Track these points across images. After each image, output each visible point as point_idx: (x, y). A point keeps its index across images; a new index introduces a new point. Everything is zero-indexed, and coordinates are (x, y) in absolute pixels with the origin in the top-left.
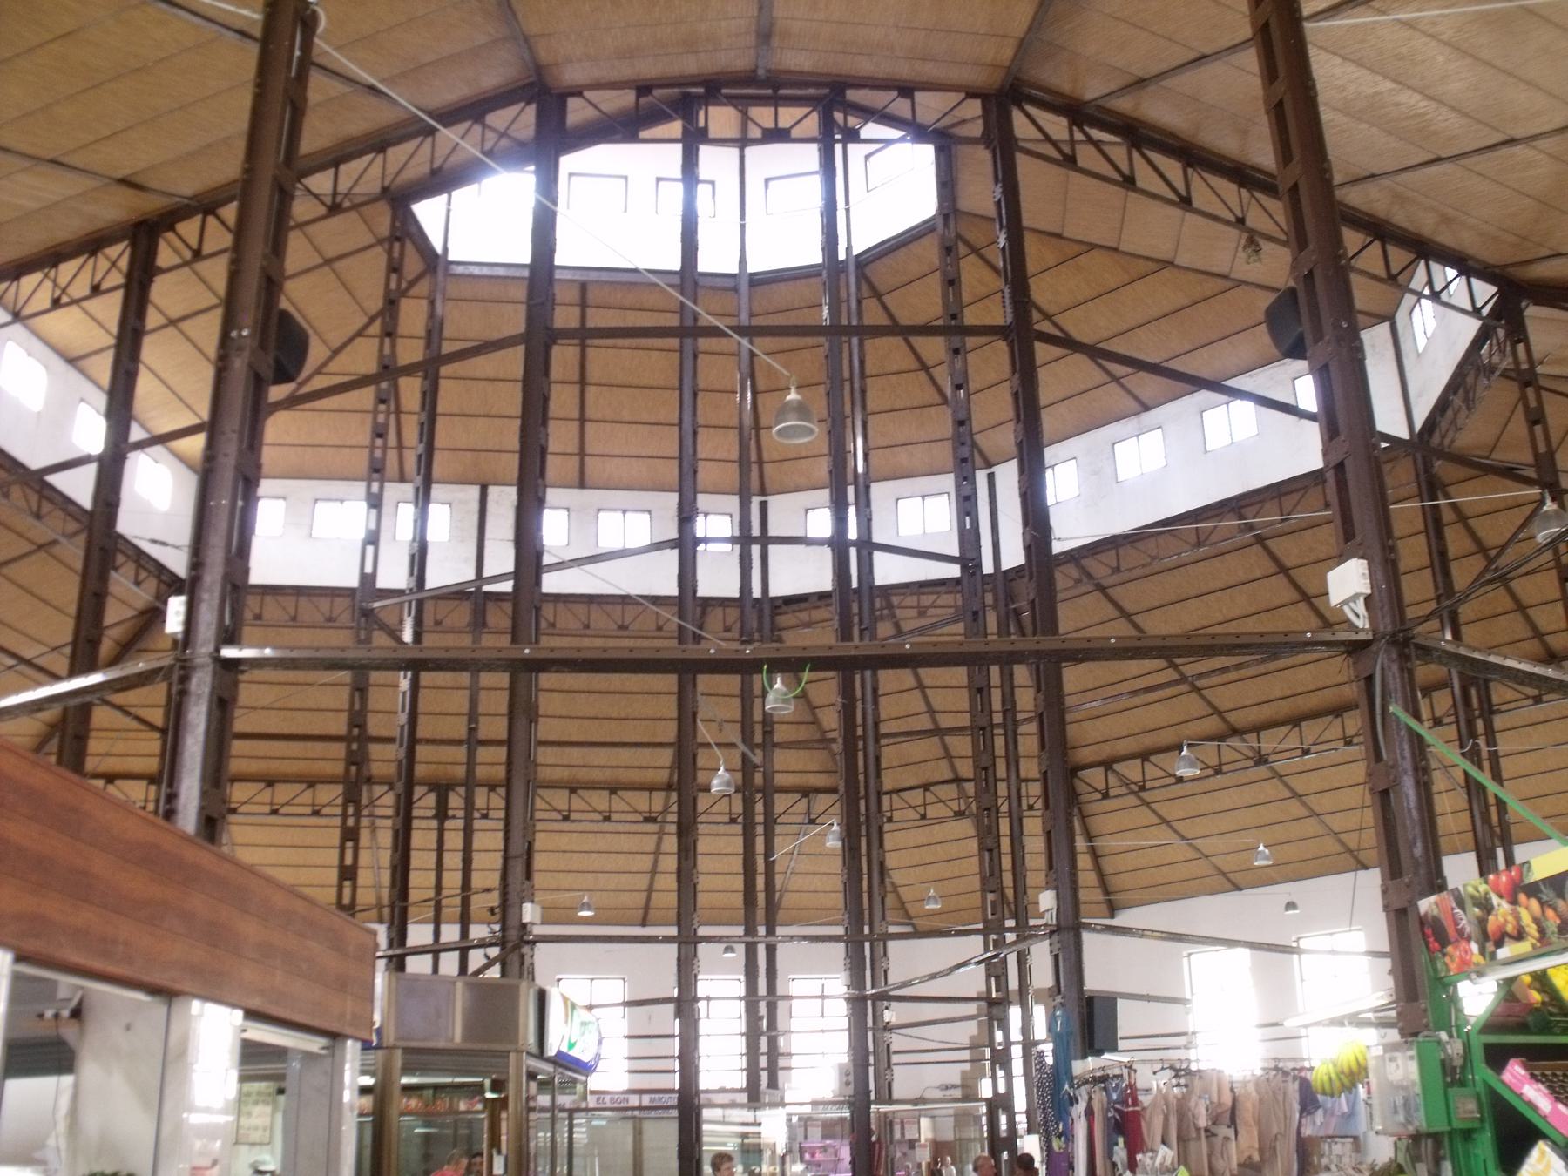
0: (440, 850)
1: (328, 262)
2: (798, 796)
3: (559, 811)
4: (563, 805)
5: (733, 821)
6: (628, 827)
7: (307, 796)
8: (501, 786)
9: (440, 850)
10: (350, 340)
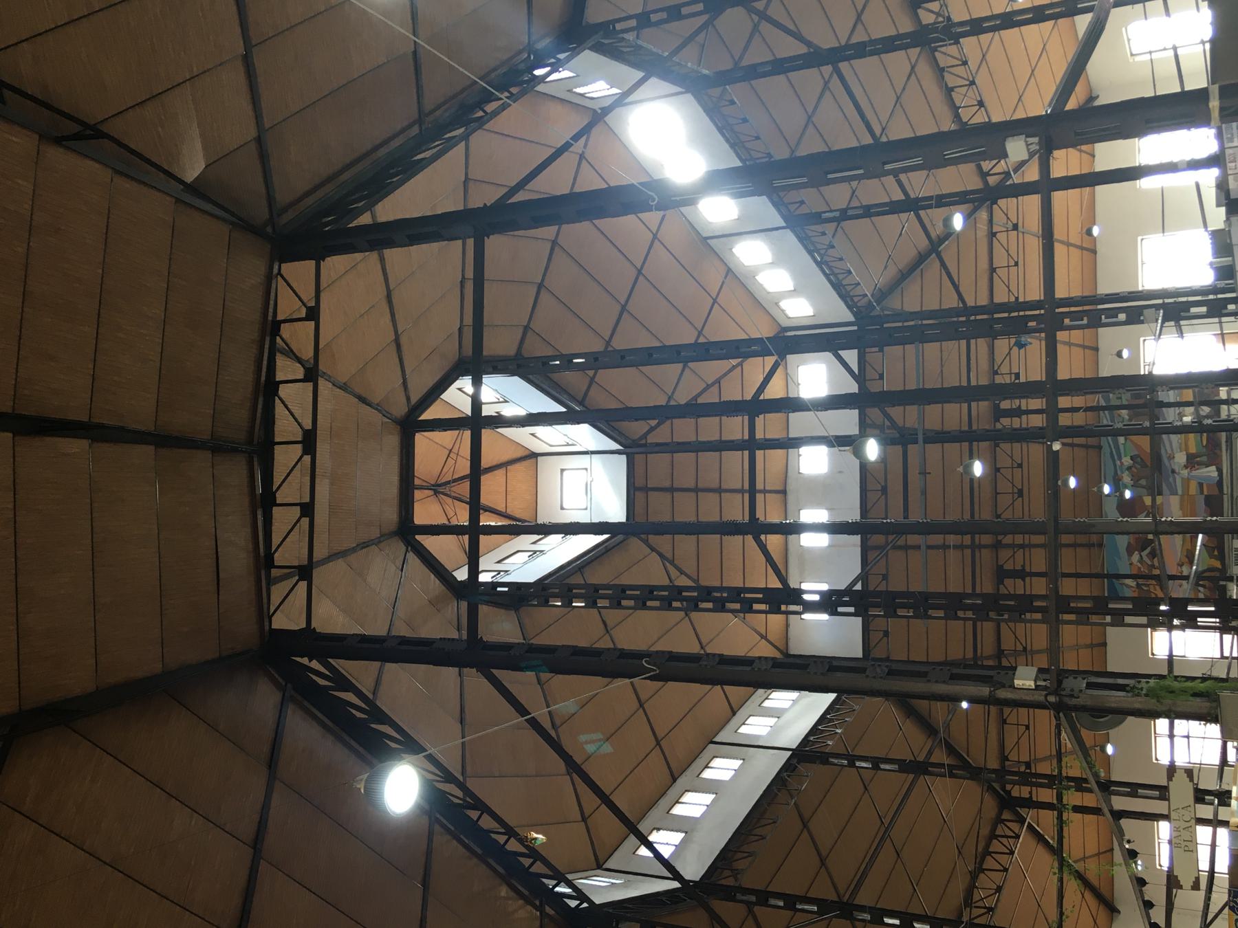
7: (1002, 273)
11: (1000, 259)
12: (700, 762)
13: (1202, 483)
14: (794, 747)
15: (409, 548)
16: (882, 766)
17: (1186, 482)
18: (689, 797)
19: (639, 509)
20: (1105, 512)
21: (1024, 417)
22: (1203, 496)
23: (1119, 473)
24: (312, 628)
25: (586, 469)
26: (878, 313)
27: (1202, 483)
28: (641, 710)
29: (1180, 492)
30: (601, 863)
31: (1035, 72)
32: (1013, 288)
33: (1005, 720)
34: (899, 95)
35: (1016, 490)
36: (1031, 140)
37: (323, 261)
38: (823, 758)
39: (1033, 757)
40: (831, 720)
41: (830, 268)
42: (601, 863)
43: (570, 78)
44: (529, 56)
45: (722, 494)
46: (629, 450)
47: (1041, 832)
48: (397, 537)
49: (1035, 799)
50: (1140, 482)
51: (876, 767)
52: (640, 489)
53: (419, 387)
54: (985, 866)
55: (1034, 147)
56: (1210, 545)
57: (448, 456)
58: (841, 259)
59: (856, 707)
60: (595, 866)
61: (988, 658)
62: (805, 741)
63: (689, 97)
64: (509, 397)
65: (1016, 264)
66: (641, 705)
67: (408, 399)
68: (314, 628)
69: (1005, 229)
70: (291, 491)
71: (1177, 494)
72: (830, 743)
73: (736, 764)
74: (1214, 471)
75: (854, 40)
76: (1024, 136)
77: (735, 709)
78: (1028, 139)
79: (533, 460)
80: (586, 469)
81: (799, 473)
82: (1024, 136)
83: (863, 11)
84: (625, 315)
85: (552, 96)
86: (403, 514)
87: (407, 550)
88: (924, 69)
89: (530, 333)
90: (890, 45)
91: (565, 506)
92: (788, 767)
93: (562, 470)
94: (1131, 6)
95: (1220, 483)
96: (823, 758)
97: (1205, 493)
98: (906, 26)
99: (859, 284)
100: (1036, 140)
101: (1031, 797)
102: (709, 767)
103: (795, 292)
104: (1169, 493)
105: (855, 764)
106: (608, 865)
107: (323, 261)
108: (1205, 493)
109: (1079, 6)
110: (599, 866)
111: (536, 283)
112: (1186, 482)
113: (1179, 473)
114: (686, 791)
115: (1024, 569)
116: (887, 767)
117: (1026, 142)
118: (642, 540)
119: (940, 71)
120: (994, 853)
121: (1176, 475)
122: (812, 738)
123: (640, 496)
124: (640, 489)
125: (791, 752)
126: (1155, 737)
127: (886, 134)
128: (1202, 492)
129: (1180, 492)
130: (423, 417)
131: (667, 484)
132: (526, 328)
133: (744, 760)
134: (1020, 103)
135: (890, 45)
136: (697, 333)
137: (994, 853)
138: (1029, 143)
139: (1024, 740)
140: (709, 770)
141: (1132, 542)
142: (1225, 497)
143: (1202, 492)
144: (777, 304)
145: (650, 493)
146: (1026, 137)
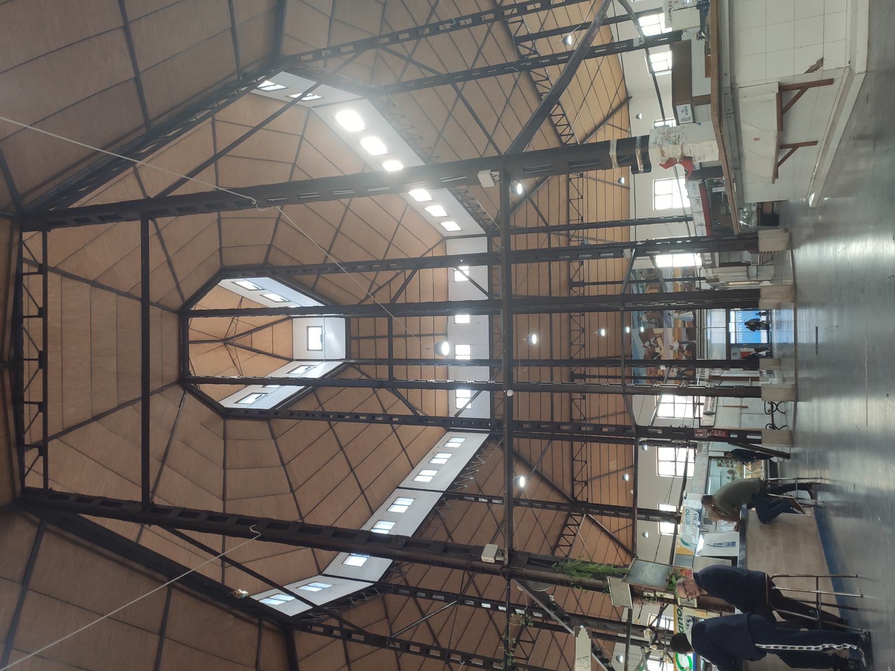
0: (600, 377)
1: (404, 449)
2: (573, 403)
3: (581, 334)
4: (578, 333)
5: (584, 398)
6: (590, 493)
7: (575, 202)
8: (570, 314)
9: (600, 377)
10: (398, 663)
11: (574, 194)
12: (389, 501)
13: (685, 321)
14: (445, 490)
15: (187, 391)
16: (494, 501)
17: (676, 320)
18: (424, 472)
19: (354, 349)
20: (634, 340)
21: (587, 287)
22: (685, 329)
23: (640, 315)
24: (49, 488)
25: (321, 327)
26: (498, 229)
27: (685, 321)
28: (394, 433)
29: (673, 327)
30: (321, 571)
31: (593, 83)
32: (581, 212)
33: (574, 458)
34: (508, 98)
35: (581, 329)
36: (494, 173)
37: (49, 232)
38: (461, 497)
39: (589, 477)
40: (468, 471)
41: (468, 204)
42: (321, 571)
43: (282, 89)
44: (239, 77)
45: (407, 338)
46: (346, 315)
47: (594, 518)
48: (177, 386)
49: (590, 502)
50: (652, 320)
51: (490, 501)
52: (355, 338)
53: (189, 291)
54: (560, 544)
55: (497, 178)
56: (688, 356)
57: (232, 321)
58: (473, 199)
59: (484, 463)
60: (317, 572)
61: (565, 424)
62: (452, 486)
63: (366, 102)
64: (265, 287)
65: (582, 197)
66: (352, 470)
67: (182, 297)
68: (51, 488)
69: (577, 177)
70: (33, 393)
71: (671, 327)
72: (466, 486)
73: (462, 440)
74: (691, 314)
75: (477, 66)
76: (490, 170)
77: (374, 510)
78: (492, 173)
79: (290, 321)
80: (321, 327)
81: (455, 323)
82: (490, 170)
83: (482, 47)
84: (339, 234)
85: (275, 99)
86: (182, 369)
87: (185, 393)
88: (523, 82)
89: (273, 249)
90: (501, 69)
91: (310, 348)
92: (440, 503)
93: (308, 327)
94: (626, 52)
95: (694, 321)
96: (461, 497)
97: (687, 327)
98: (512, 58)
99: (485, 213)
100: (497, 173)
101: (588, 501)
102: (374, 528)
103: (448, 218)
104: (666, 326)
105: (478, 500)
106: (326, 572)
107: (49, 232)
108: (687, 327)
109: (596, 52)
110: (320, 573)
111: (274, 218)
112: (676, 320)
113: (672, 316)
114: (379, 520)
115: (585, 374)
116: (496, 501)
117: (491, 175)
118: (356, 369)
119: (534, 84)
120: (565, 535)
121: (671, 317)
122: (456, 484)
123: (354, 343)
124: (355, 338)
125: (442, 493)
126: (658, 462)
127: (501, 122)
128: (685, 326)
129: (673, 327)
130: (193, 309)
131: (372, 334)
132: (270, 246)
133: (415, 499)
134: (585, 101)
135: (501, 69)
136: (388, 243)
137: (565, 535)
138: (494, 175)
139: (584, 469)
140: (394, 506)
141: (647, 354)
142: (697, 329)
143: (685, 326)
144: (439, 224)
145: (361, 340)
146: (492, 171)
